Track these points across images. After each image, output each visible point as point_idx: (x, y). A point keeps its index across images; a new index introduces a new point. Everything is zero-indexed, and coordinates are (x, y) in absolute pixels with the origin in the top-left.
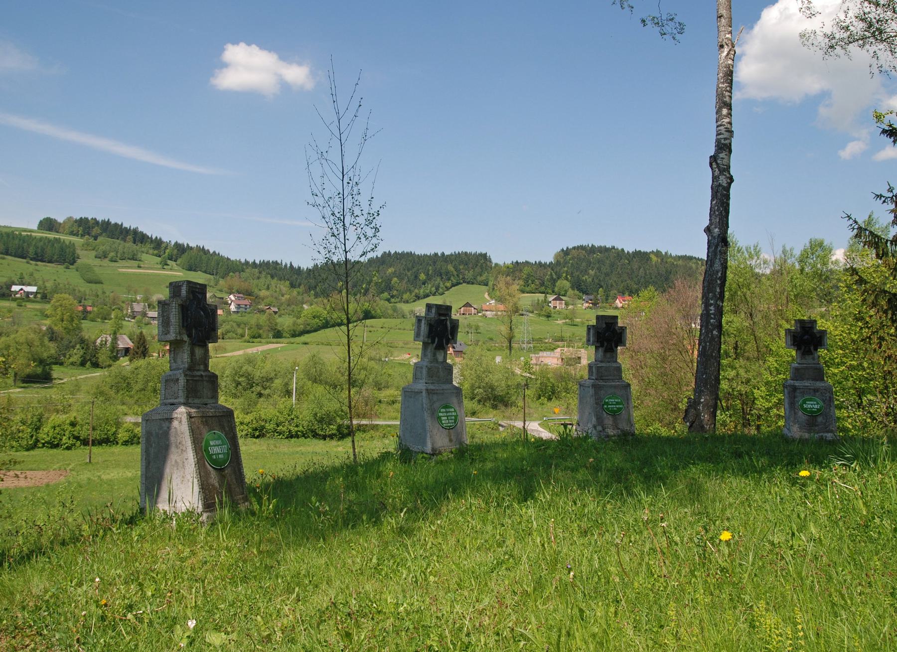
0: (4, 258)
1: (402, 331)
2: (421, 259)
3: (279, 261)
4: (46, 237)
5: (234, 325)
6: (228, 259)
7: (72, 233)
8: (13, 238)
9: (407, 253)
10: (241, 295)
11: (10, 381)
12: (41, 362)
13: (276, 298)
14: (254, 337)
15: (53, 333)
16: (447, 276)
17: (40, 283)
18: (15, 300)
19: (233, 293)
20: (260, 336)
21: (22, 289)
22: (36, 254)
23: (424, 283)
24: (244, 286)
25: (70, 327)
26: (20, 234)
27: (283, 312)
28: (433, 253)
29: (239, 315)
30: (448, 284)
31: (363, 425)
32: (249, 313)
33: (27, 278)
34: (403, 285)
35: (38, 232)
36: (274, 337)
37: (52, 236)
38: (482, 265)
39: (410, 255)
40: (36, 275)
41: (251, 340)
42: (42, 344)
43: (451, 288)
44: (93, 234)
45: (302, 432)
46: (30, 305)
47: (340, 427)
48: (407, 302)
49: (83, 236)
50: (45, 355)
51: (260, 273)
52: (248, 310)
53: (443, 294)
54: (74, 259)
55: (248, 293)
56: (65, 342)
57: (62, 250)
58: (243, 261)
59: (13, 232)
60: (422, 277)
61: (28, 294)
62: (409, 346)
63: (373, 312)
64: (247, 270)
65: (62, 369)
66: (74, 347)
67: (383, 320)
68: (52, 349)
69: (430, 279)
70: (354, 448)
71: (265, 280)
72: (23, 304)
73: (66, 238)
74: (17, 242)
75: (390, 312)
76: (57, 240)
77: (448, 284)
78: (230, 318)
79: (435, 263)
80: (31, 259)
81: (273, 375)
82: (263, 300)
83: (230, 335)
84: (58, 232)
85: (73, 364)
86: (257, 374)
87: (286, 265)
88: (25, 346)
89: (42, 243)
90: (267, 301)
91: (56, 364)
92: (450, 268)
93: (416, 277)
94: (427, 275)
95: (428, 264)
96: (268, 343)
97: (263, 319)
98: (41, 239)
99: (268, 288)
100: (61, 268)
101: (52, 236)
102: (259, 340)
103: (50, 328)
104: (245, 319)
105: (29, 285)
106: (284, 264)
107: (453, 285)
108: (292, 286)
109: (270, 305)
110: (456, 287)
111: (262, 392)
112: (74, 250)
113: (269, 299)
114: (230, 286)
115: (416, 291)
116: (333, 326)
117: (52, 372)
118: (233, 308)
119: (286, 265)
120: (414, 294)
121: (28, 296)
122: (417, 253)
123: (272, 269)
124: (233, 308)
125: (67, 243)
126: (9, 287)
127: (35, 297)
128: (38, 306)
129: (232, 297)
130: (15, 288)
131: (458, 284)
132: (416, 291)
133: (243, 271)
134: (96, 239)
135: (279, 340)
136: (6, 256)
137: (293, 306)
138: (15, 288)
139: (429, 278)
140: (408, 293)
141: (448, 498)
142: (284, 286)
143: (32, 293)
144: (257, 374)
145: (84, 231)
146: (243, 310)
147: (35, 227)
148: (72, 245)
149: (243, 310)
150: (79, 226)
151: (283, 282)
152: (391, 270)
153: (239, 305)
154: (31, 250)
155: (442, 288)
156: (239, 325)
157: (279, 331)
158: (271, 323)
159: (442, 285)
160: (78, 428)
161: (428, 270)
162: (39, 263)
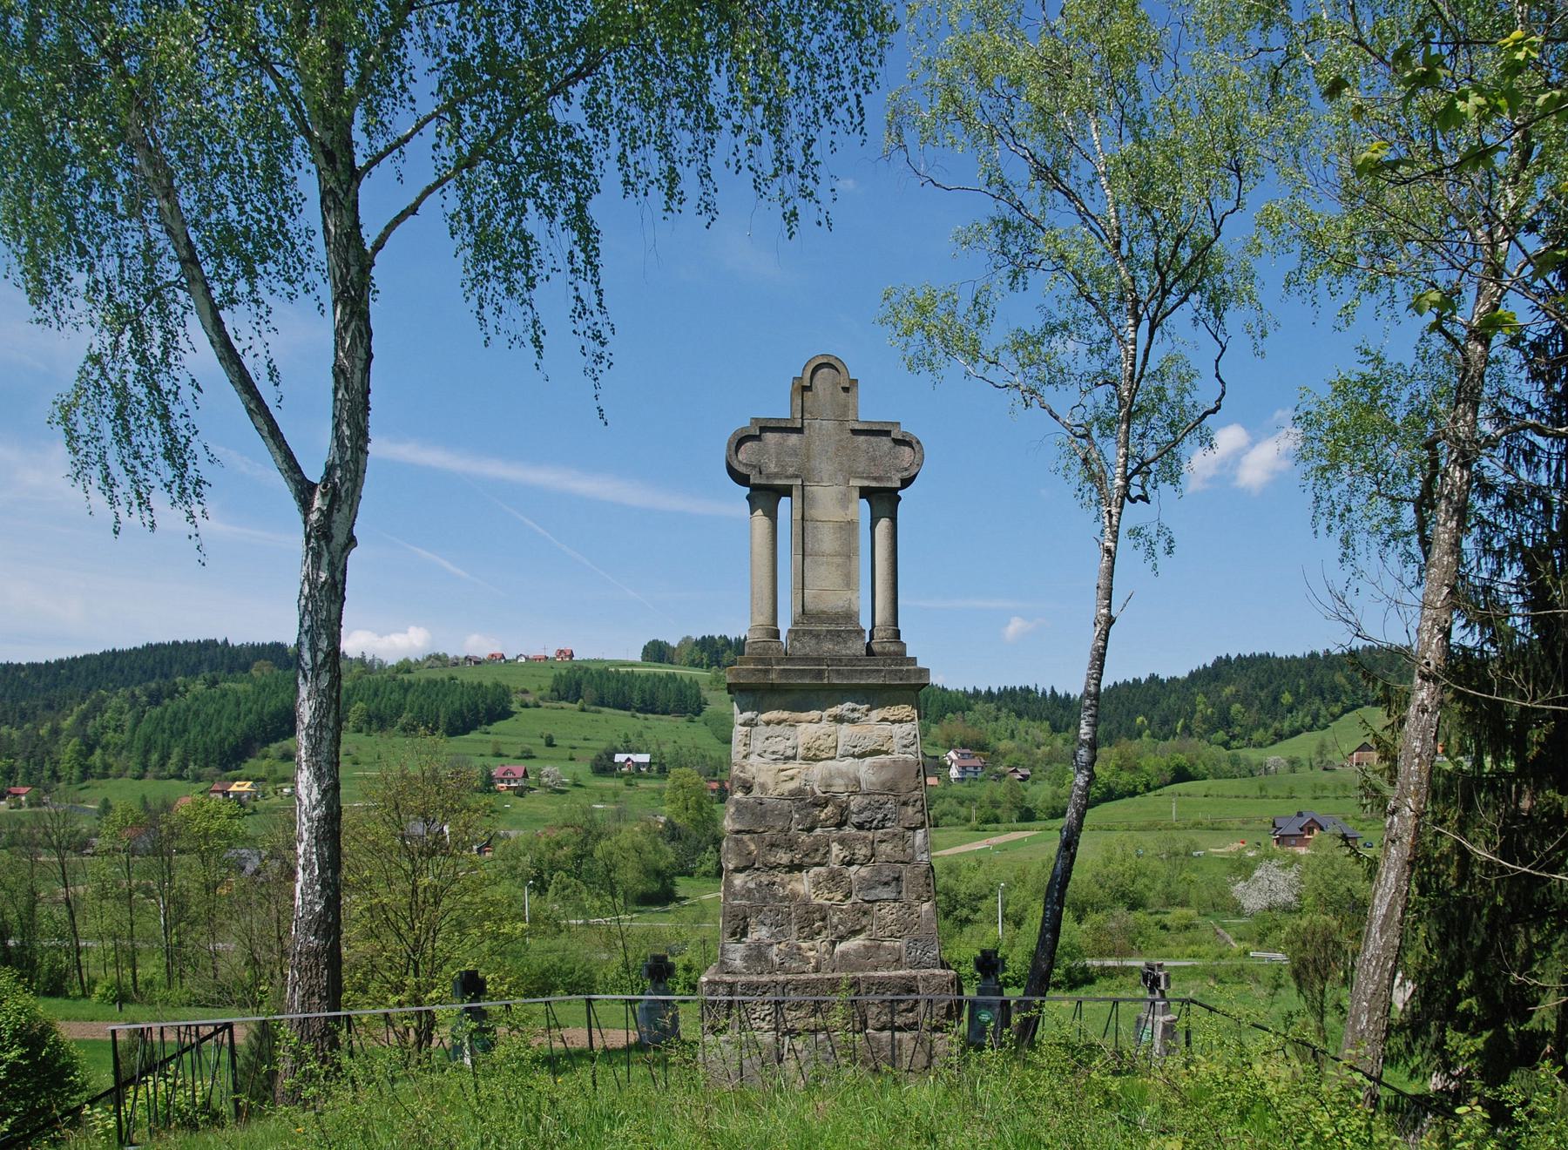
0: (599, 712)
1: (1242, 800)
2: (1285, 665)
3: (1032, 687)
5: (954, 802)
6: (944, 690)
7: (694, 664)
8: (608, 678)
9: (1261, 656)
10: (968, 751)
11: (620, 901)
12: (659, 874)
13: (1026, 752)
14: (987, 822)
15: (675, 829)
16: (1335, 693)
17: (654, 747)
18: (622, 776)
19: (955, 747)
20: (997, 820)
21: (629, 759)
22: (643, 701)
23: (1290, 711)
24: (972, 734)
25: (699, 818)
26: (618, 672)
27: (1039, 775)
28: (1308, 652)
29: (966, 783)
30: (1336, 709)
31: (1109, 967)
32: (982, 780)
33: (634, 742)
34: (1251, 717)
36: (1020, 820)
37: (663, 670)
38: (1400, 669)
39: (1265, 658)
40: (648, 736)
41: (981, 827)
42: (657, 850)
43: (1341, 715)
45: (1013, 979)
46: (643, 784)
47: (1069, 971)
48: (1260, 745)
49: (709, 666)
50: (662, 864)
51: (999, 709)
52: (980, 775)
53: (1326, 727)
54: (699, 706)
55: (980, 747)
56: (692, 842)
57: (680, 692)
58: (970, 690)
59: (606, 669)
60: (1287, 698)
61: (638, 765)
62: (1251, 826)
63: (1191, 769)
64: (977, 707)
65: (692, 882)
66: (705, 850)
67: (1209, 782)
68: (669, 854)
69: (1301, 702)
71: (1007, 721)
72: (634, 781)
73: (685, 672)
74: (613, 684)
75: (1225, 766)
76: (671, 677)
77: (1336, 709)
78: (949, 790)
79: (1310, 671)
80: (638, 711)
81: (986, 891)
82: (1004, 757)
83: (946, 819)
84: (672, 663)
85: (705, 874)
86: (963, 890)
87: (1044, 693)
88: (633, 853)
89: (649, 684)
90: (1012, 758)
91: (681, 874)
92: (1340, 678)
93: (1276, 700)
94: (1296, 694)
95: (1297, 674)
96: (1008, 830)
97: (1000, 790)
98: (648, 677)
99: (1012, 736)
100: (681, 722)
101: (663, 670)
102: (994, 825)
103: (670, 825)
104: (971, 791)
105: (639, 751)
106: (1040, 692)
107: (1346, 711)
108: (1055, 729)
109: (1016, 765)
110: (1351, 714)
111: (971, 917)
112: (698, 692)
113: (1013, 756)
114: (948, 735)
115: (1277, 725)
116: (1121, 796)
117: (676, 889)
118: (954, 773)
119: (1044, 693)
120: (1271, 731)
121: (639, 770)
122: (1278, 656)
123: (1019, 702)
124: (954, 773)
126: (611, 757)
127: (649, 770)
128: (654, 784)
129: (952, 754)
130: (620, 758)
131: (1354, 707)
132: (1277, 725)
133: (969, 709)
135: (1026, 824)
137: (1055, 765)
138: (620, 758)
139: (1299, 700)
140: (1261, 730)
141: (253, 1054)
142: (1040, 731)
143: (644, 764)
144: (963, 890)
145: (710, 658)
146: (972, 775)
148: (694, 684)
149: (972, 775)
150: (703, 651)
151: (1038, 723)
152: (1229, 690)
153: (964, 768)
154: (636, 696)
155: (1325, 717)
156: (961, 803)
157: (1028, 810)
158: (1015, 798)
159: (1323, 712)
160: (694, 974)
161: (1299, 686)
162: (650, 716)
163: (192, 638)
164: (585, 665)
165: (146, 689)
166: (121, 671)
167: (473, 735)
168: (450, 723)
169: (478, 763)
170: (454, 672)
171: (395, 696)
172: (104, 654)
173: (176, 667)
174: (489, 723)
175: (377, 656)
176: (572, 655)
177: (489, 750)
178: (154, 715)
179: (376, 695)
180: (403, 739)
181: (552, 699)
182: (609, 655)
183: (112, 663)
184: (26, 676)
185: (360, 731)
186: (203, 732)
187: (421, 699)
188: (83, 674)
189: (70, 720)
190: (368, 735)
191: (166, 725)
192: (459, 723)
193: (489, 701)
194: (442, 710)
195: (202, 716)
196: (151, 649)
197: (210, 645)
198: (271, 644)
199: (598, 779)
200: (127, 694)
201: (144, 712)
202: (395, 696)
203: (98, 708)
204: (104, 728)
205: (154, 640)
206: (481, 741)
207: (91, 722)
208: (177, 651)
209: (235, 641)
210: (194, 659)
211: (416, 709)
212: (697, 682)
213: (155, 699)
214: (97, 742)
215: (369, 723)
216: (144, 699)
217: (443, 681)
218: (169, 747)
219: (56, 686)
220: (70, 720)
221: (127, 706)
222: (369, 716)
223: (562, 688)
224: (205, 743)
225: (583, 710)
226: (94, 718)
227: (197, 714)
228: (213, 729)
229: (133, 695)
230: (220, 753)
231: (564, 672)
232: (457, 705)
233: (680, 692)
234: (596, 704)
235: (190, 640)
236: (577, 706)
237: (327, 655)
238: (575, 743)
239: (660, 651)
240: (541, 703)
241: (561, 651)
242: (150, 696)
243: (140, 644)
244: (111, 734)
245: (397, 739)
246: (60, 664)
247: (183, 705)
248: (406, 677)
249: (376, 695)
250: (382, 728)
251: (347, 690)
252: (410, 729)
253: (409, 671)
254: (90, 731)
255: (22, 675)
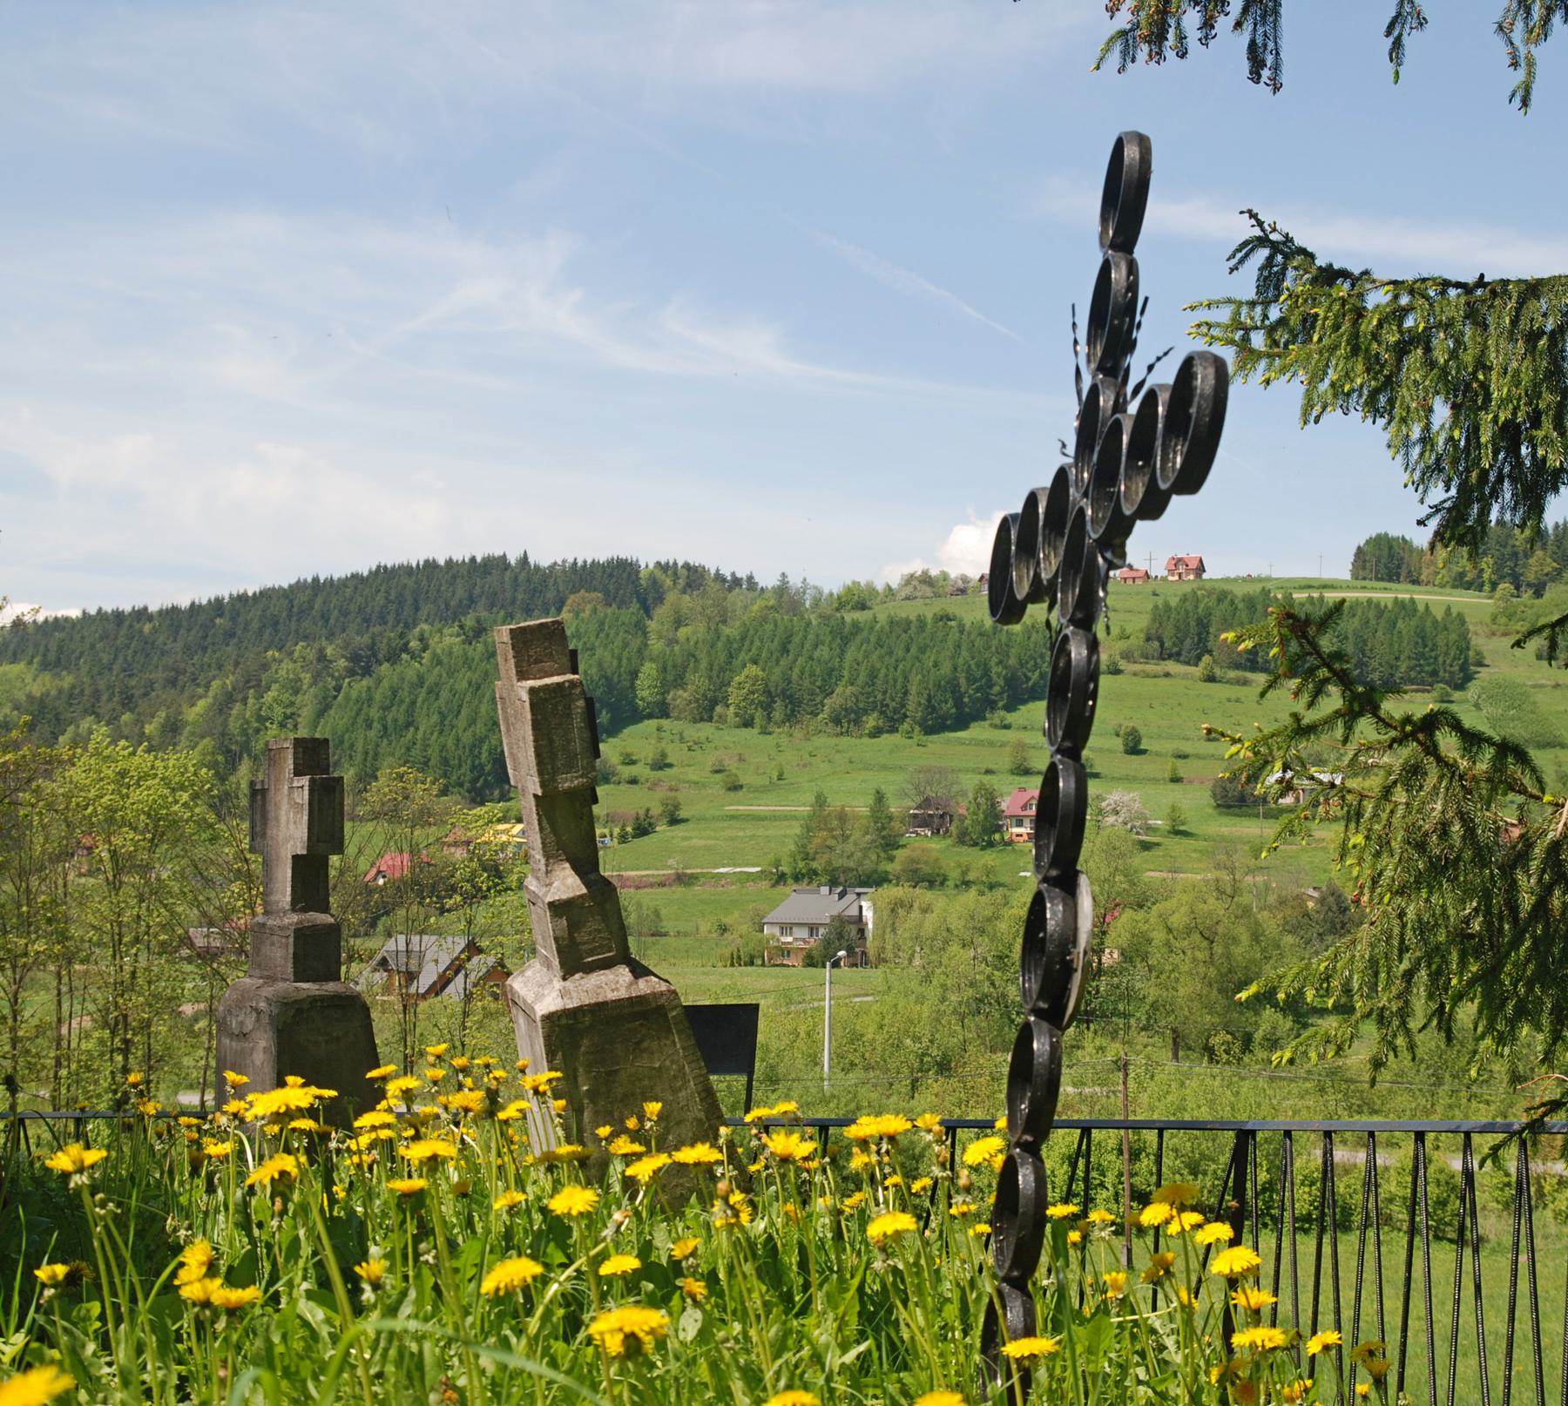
0: (1245, 683)
4: (1370, 601)
26: (1288, 598)
35: (1355, 588)
37: (1386, 594)
44: (1531, 576)
59: (1266, 592)
70: (1509, 1366)
76: (1406, 608)
84: (1416, 582)
101: (1386, 594)
112: (1464, 636)
125: (1439, 614)
134: (1538, 594)
136: (1249, 675)
145: (1498, 569)
147: (1341, 570)
163: (460, 554)
164: (1226, 587)
165: (347, 645)
166: (325, 618)
167: (977, 731)
168: (930, 707)
169: (969, 782)
170: (953, 606)
171: (823, 652)
172: (299, 587)
173: (426, 609)
174: (1011, 708)
175: (811, 582)
176: (1201, 569)
177: (1004, 760)
178: (354, 694)
179: (785, 650)
180: (833, 741)
181: (1146, 657)
182: (1258, 568)
183: (311, 601)
184: (155, 631)
185: (748, 723)
186: (442, 727)
187: (874, 657)
188: (255, 625)
189: (201, 705)
190: (765, 732)
191: (375, 713)
192: (948, 707)
193: (1012, 661)
194: (915, 679)
195: (445, 694)
196: (384, 575)
197: (495, 565)
198: (610, 563)
199: (1225, 820)
200: (312, 655)
201: (338, 689)
202: (823, 652)
203: (255, 682)
204: (262, 720)
205: (393, 558)
206: (992, 744)
207: (238, 707)
208: (429, 579)
209: (542, 557)
210: (461, 592)
211: (862, 679)
212: (1461, 618)
213: (362, 664)
214: (246, 747)
215: (768, 708)
216: (342, 663)
217: (921, 622)
218: (376, 755)
219: (204, 649)
220: (201, 705)
221: (307, 677)
222: (768, 692)
223: (1168, 634)
224: (443, 747)
225: (1211, 679)
226: (244, 701)
227: (434, 692)
228: (462, 722)
229: (322, 657)
230: (473, 768)
231: (1174, 602)
232: (946, 669)
233: (1421, 635)
234: (1238, 666)
235: (458, 557)
236: (1197, 671)
237: (1464, 838)
238: (1187, 748)
239: (1391, 556)
240: (1123, 665)
241: (1178, 562)
242: (354, 658)
243: (364, 565)
244: (273, 730)
245: (820, 741)
246: (217, 606)
247: (411, 675)
248: (859, 616)
249: (785, 650)
250: (791, 718)
251: (729, 641)
252: (846, 720)
253: (863, 606)
254: (234, 726)
255: (147, 628)
